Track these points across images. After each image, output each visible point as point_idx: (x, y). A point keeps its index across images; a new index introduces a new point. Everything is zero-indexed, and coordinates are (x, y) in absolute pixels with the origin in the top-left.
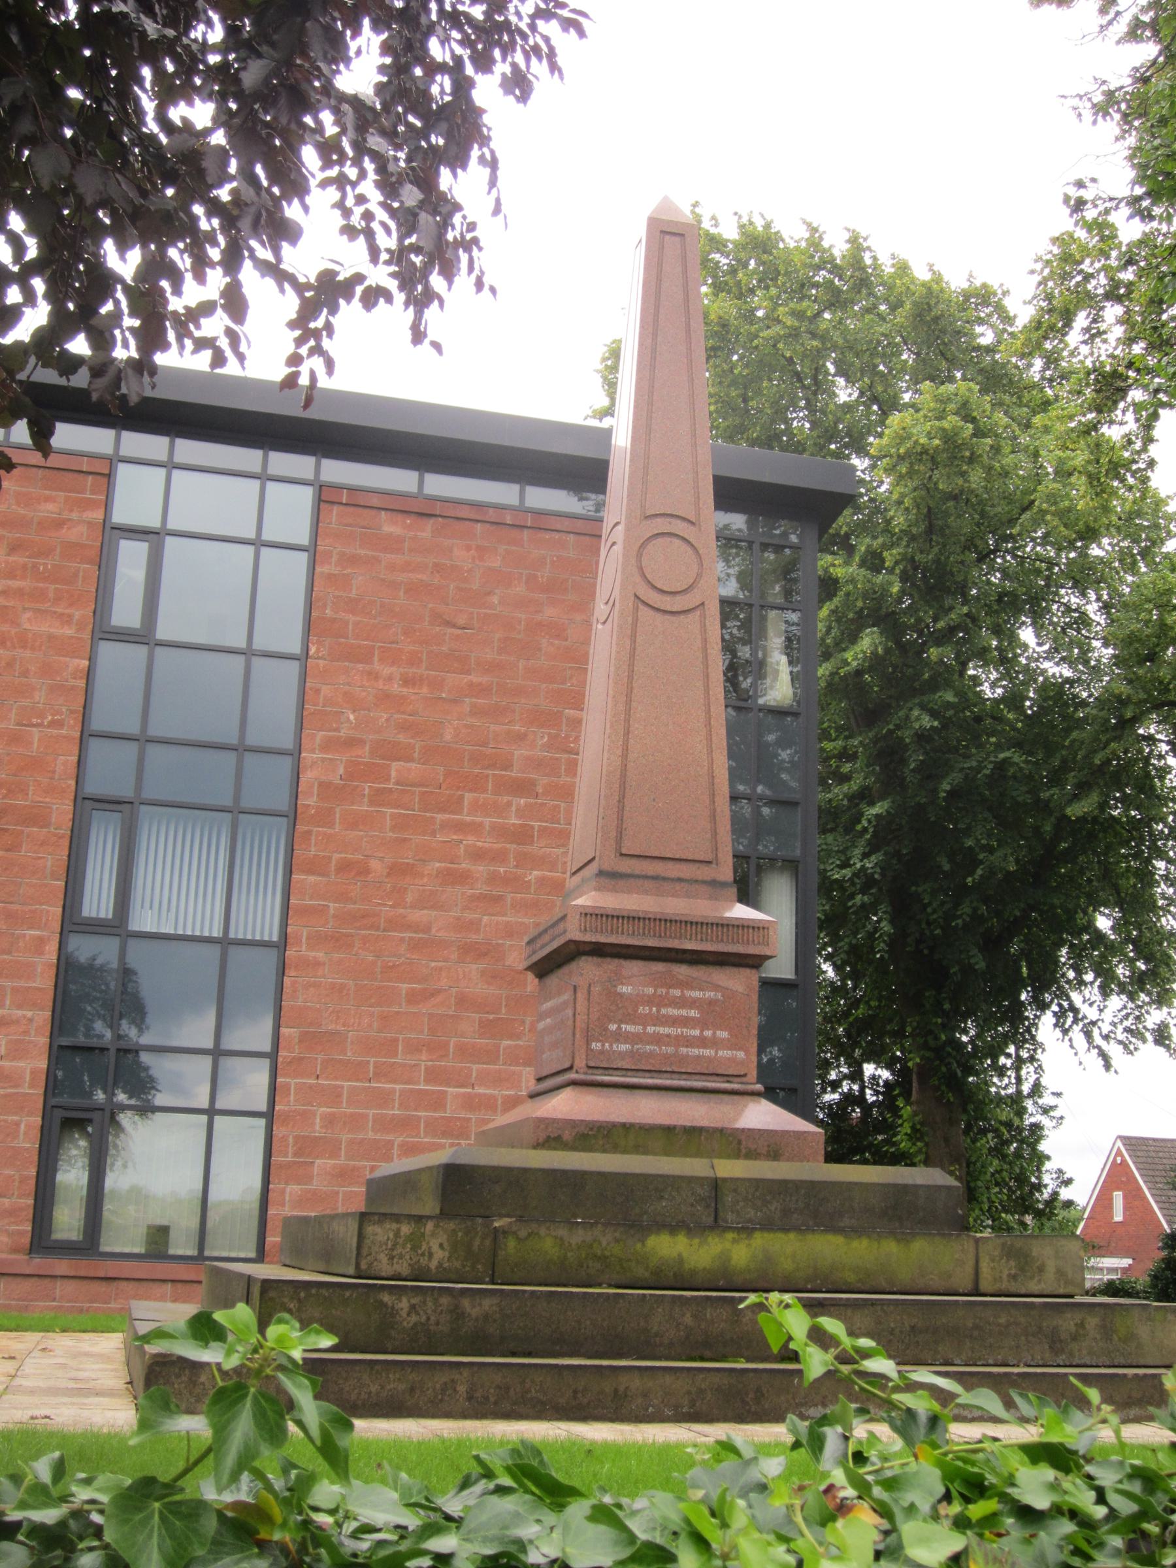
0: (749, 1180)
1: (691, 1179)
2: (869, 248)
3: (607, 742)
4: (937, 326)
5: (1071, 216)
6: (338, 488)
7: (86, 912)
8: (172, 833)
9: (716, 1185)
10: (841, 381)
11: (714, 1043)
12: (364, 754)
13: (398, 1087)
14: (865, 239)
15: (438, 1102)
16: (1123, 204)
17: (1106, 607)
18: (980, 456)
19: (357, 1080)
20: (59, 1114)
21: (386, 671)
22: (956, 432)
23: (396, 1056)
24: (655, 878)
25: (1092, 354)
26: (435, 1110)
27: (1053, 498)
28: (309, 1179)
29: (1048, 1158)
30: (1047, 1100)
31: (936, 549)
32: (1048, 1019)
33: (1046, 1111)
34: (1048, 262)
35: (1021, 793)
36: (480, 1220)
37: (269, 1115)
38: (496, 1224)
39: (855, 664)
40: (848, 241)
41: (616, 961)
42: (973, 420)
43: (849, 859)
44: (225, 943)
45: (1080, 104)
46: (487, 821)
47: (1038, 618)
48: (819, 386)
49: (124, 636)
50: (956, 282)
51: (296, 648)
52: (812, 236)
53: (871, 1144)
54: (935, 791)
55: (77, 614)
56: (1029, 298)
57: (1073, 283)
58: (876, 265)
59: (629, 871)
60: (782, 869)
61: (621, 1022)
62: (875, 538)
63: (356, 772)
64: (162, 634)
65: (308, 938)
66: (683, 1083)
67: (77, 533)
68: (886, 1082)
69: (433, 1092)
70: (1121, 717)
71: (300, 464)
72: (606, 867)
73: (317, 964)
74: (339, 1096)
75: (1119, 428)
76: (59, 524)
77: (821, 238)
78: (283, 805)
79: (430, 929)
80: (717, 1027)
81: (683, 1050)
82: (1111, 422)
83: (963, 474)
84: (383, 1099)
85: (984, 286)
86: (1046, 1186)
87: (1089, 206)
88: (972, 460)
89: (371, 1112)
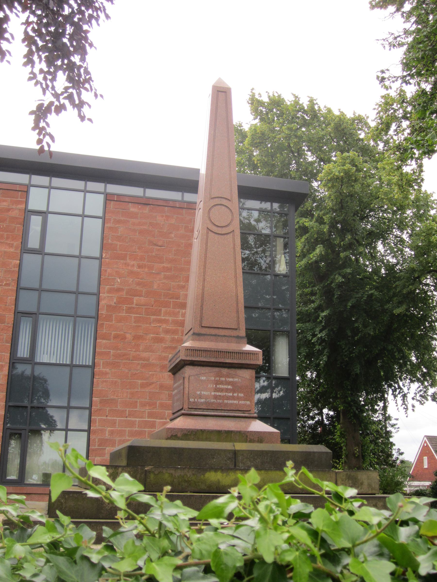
0: (248, 451)
1: (225, 451)
2: (317, 104)
3: (197, 283)
4: (343, 132)
5: (380, 84)
6: (114, 195)
7: (19, 355)
8: (61, 328)
9: (235, 453)
10: (309, 153)
11: (238, 398)
12: (124, 294)
13: (137, 419)
14: (316, 100)
15: (153, 425)
16: (399, 79)
17: (411, 236)
18: (359, 179)
19: (122, 417)
20: (9, 432)
21: (132, 263)
22: (349, 170)
23: (136, 408)
24: (215, 335)
25: (398, 139)
26: (152, 428)
27: (386, 194)
28: (104, 455)
29: (394, 445)
30: (393, 422)
31: (344, 215)
32: (390, 392)
33: (393, 426)
34: (380, 105)
35: (377, 306)
36: (139, 467)
37: (89, 431)
38: (146, 469)
39: (314, 258)
40: (309, 101)
41: (199, 367)
42: (356, 166)
43: (315, 332)
44: (72, 366)
45: (384, 43)
46: (171, 318)
47: (385, 239)
48: (300, 154)
49: (33, 251)
50: (349, 115)
51: (98, 255)
52: (295, 99)
53: (326, 440)
54: (346, 306)
55: (15, 244)
56: (373, 119)
57: (390, 113)
58: (320, 110)
59: (205, 333)
60: (282, 335)
61: (201, 390)
62: (321, 211)
63: (121, 301)
64: (47, 250)
65: (103, 364)
66: (225, 414)
67: (15, 213)
68: (332, 416)
69: (151, 421)
70: (415, 276)
71: (99, 186)
72: (196, 331)
73: (106, 373)
74: (115, 423)
75: (409, 168)
76: (8, 210)
77: (299, 100)
78: (93, 314)
79: (149, 360)
80: (239, 392)
81: (226, 401)
82: (407, 165)
83: (352, 186)
84: (132, 424)
85: (359, 116)
86: (393, 455)
87: (387, 80)
88: (356, 180)
89: (127, 429)
